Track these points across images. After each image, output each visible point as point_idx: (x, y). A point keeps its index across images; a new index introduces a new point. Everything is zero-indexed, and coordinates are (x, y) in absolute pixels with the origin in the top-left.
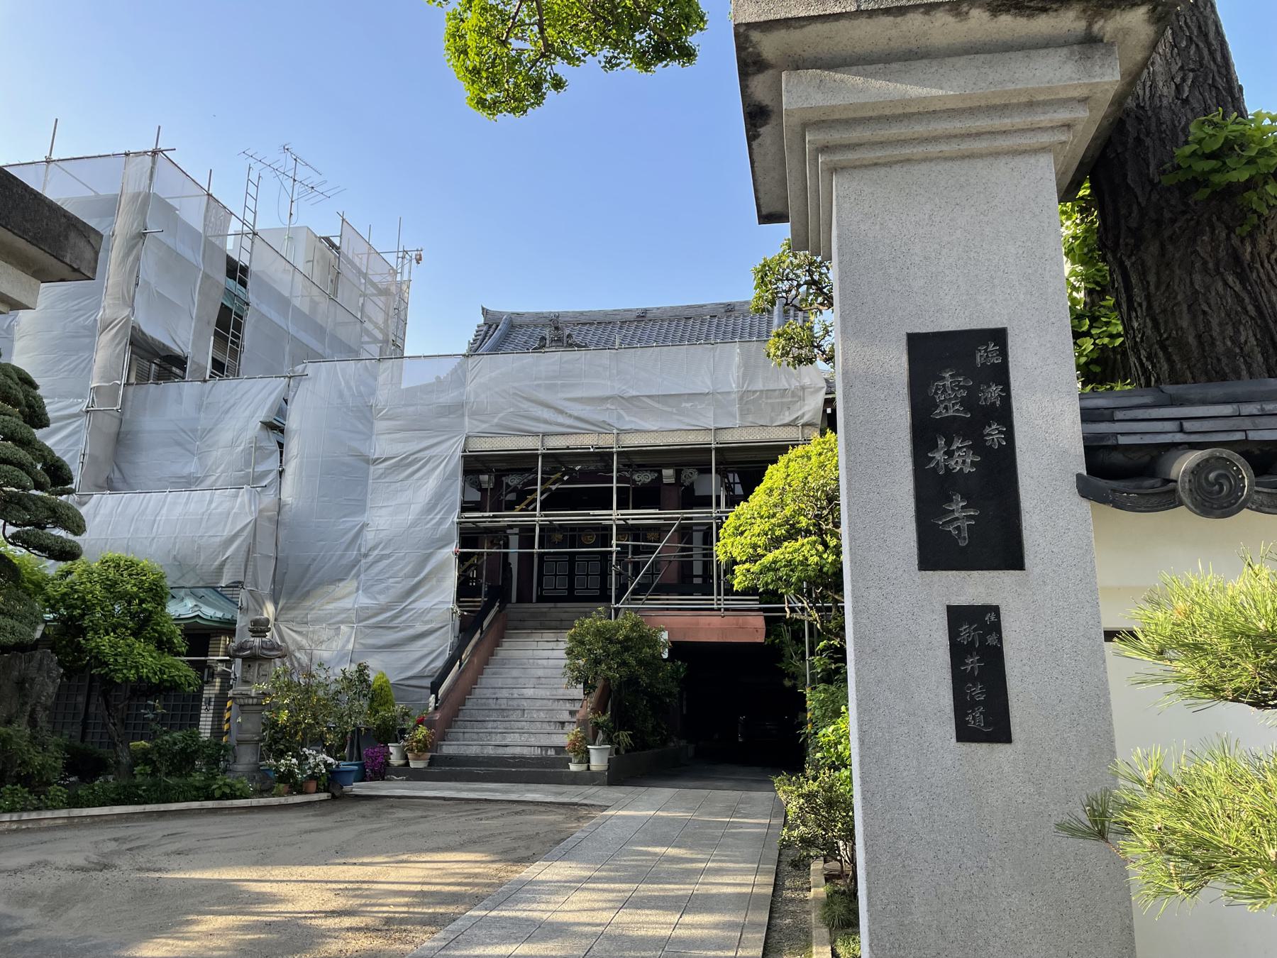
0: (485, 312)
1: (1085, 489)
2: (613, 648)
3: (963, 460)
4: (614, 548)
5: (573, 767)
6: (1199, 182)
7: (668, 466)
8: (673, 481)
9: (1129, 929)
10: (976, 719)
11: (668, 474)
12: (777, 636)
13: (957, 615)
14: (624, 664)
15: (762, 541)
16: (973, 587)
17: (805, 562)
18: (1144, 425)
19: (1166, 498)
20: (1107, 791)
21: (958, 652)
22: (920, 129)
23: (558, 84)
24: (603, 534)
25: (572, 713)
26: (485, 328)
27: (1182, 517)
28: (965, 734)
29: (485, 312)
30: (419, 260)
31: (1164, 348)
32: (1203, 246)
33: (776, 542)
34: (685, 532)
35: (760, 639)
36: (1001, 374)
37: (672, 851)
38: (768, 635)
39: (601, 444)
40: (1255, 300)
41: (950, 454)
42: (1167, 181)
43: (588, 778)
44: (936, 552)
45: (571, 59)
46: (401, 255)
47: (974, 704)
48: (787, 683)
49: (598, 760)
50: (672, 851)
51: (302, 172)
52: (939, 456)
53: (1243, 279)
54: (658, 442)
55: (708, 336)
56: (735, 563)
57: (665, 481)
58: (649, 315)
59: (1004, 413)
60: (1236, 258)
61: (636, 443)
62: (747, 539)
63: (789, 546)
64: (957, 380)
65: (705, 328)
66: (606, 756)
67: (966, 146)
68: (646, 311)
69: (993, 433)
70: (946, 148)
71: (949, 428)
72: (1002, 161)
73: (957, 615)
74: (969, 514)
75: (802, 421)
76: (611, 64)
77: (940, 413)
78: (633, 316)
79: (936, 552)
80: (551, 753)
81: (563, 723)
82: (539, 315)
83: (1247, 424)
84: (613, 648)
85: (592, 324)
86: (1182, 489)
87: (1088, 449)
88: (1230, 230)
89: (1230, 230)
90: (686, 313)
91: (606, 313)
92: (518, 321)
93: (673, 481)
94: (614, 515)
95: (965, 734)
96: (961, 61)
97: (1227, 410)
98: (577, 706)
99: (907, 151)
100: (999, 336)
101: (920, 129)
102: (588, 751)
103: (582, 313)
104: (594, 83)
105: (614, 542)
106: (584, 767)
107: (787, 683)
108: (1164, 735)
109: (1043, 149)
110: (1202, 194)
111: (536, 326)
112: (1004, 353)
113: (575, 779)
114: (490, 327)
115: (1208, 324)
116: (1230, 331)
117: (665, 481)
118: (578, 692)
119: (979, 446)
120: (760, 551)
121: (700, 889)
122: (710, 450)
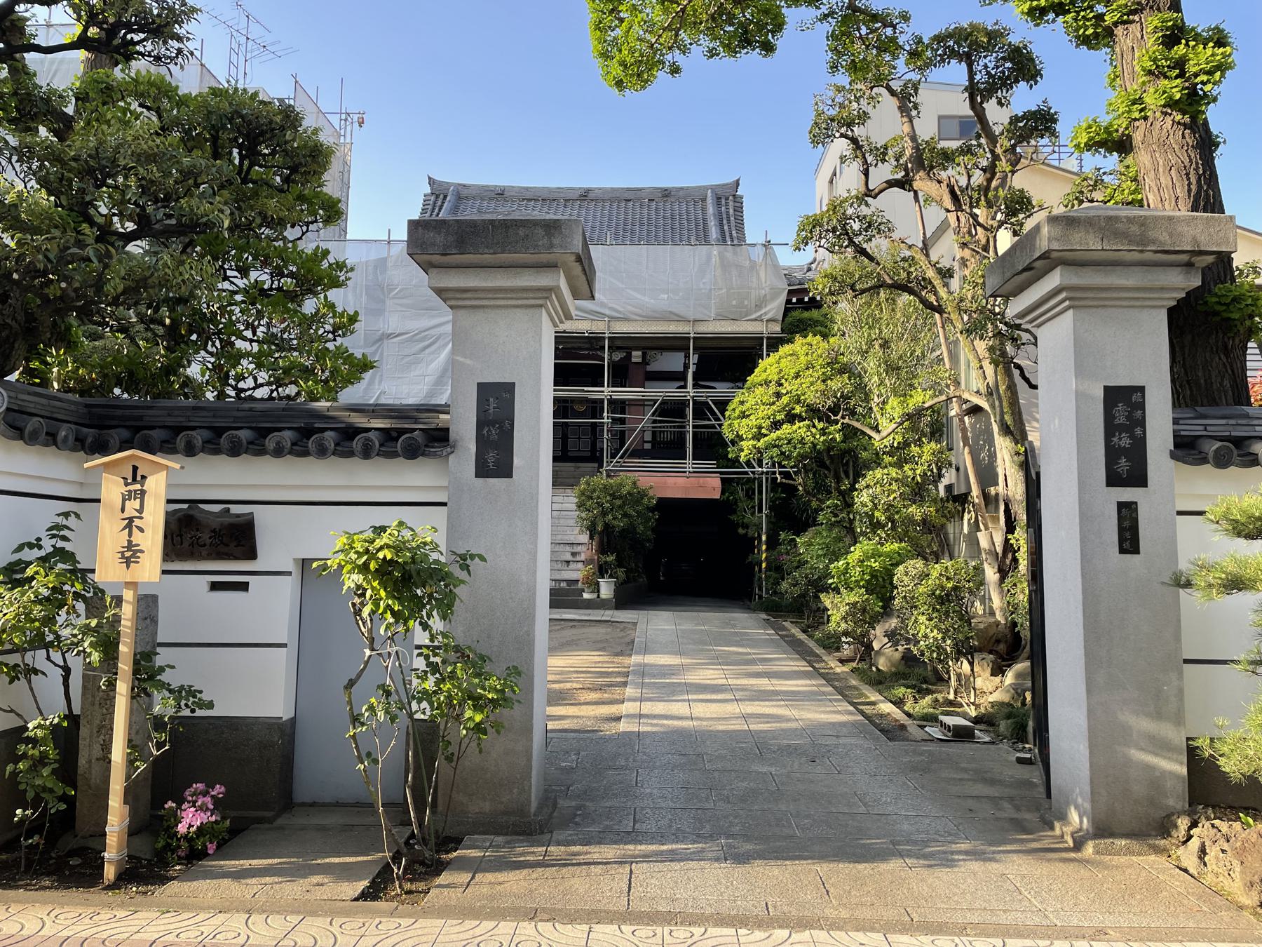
0: (431, 181)
1: (1173, 456)
2: (618, 502)
3: (1125, 442)
4: (605, 420)
5: (586, 596)
6: (1216, 313)
7: (637, 349)
8: (640, 360)
9: (1179, 621)
10: (1127, 545)
11: (637, 356)
12: (732, 494)
13: (1121, 506)
14: (625, 515)
15: (766, 423)
16: (1127, 494)
17: (802, 441)
18: (1193, 428)
19: (1203, 460)
20: (1174, 573)
21: (1120, 519)
22: (1115, 295)
23: (675, 70)
24: (595, 407)
25: (574, 554)
26: (433, 198)
27: (1208, 468)
28: (1122, 551)
29: (431, 181)
30: (361, 124)
31: (1188, 382)
32: (1212, 340)
33: (776, 425)
34: (701, 410)
35: (717, 496)
36: (1142, 406)
37: (741, 650)
38: (723, 493)
39: (594, 329)
40: (1231, 366)
41: (1120, 439)
42: (1201, 308)
43: (599, 604)
44: (1114, 480)
45: (684, 50)
46: (343, 117)
47: (1126, 540)
48: (741, 531)
49: (607, 589)
50: (741, 650)
51: (255, 31)
52: (1116, 439)
53: (1227, 357)
54: (644, 330)
55: (689, 238)
56: (741, 438)
57: (634, 360)
58: (591, 195)
59: (1142, 423)
60: (1226, 347)
61: (625, 330)
62: (753, 421)
63: (786, 429)
64: (1123, 405)
65: (645, 211)
66: (613, 587)
67: (1132, 303)
68: (588, 191)
69: (1138, 431)
70: (1124, 303)
71: (1121, 428)
72: (1145, 310)
73: (1121, 506)
74: (1125, 465)
75: (767, 317)
76: (712, 53)
77: (1117, 421)
78: (576, 196)
79: (1114, 480)
80: (563, 585)
81: (568, 562)
82: (485, 188)
83: (1231, 428)
84: (618, 502)
85: (537, 200)
86: (1211, 455)
87: (1175, 436)
88: (1225, 334)
89: (1225, 334)
90: (627, 195)
91: (550, 190)
92: (465, 193)
93: (640, 360)
94: (606, 392)
95: (1122, 551)
96: (1136, 269)
97: (1223, 422)
98: (579, 549)
99: (1107, 303)
100: (1141, 389)
101: (1115, 295)
102: (598, 583)
103: (527, 189)
104: (702, 66)
105: (605, 414)
106: (595, 595)
107: (741, 531)
108: (1206, 546)
109: (1163, 306)
110: (1217, 319)
111: (483, 199)
112: (1143, 397)
113: (588, 605)
114: (437, 197)
115: (1210, 377)
116: (1219, 379)
117: (634, 360)
118: (585, 538)
119: (1132, 437)
120: (764, 431)
121: (775, 668)
122: (689, 338)
